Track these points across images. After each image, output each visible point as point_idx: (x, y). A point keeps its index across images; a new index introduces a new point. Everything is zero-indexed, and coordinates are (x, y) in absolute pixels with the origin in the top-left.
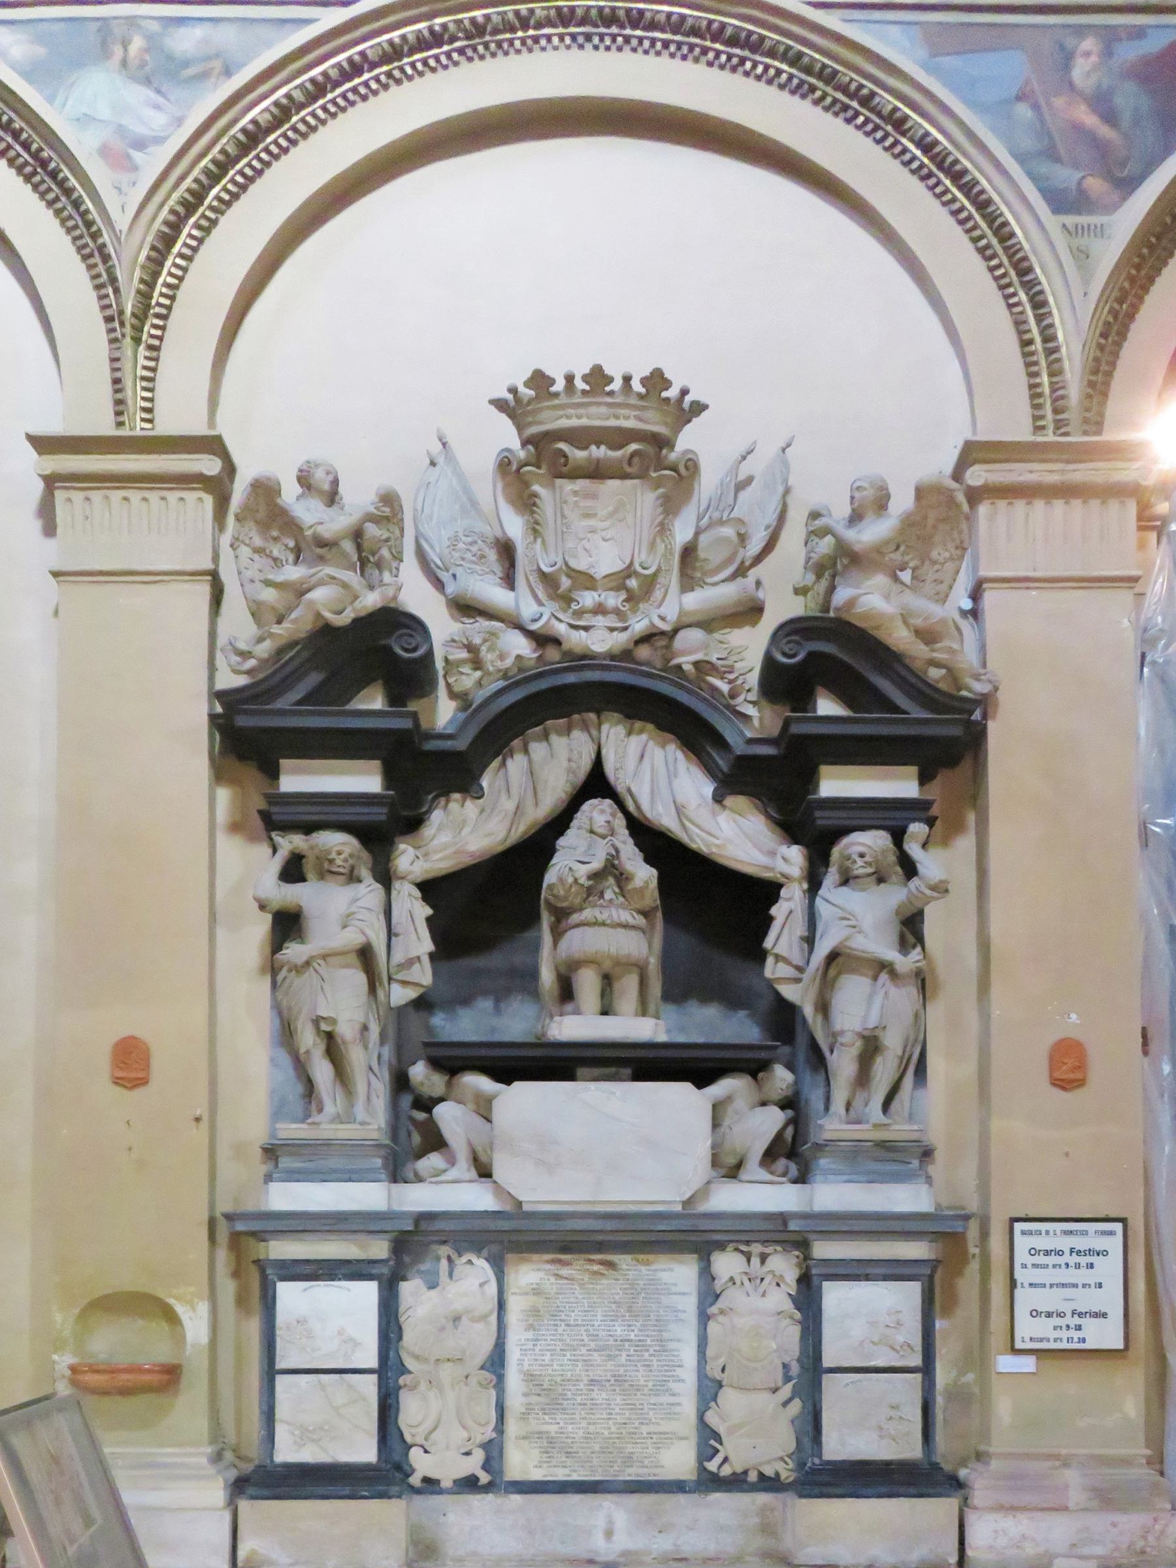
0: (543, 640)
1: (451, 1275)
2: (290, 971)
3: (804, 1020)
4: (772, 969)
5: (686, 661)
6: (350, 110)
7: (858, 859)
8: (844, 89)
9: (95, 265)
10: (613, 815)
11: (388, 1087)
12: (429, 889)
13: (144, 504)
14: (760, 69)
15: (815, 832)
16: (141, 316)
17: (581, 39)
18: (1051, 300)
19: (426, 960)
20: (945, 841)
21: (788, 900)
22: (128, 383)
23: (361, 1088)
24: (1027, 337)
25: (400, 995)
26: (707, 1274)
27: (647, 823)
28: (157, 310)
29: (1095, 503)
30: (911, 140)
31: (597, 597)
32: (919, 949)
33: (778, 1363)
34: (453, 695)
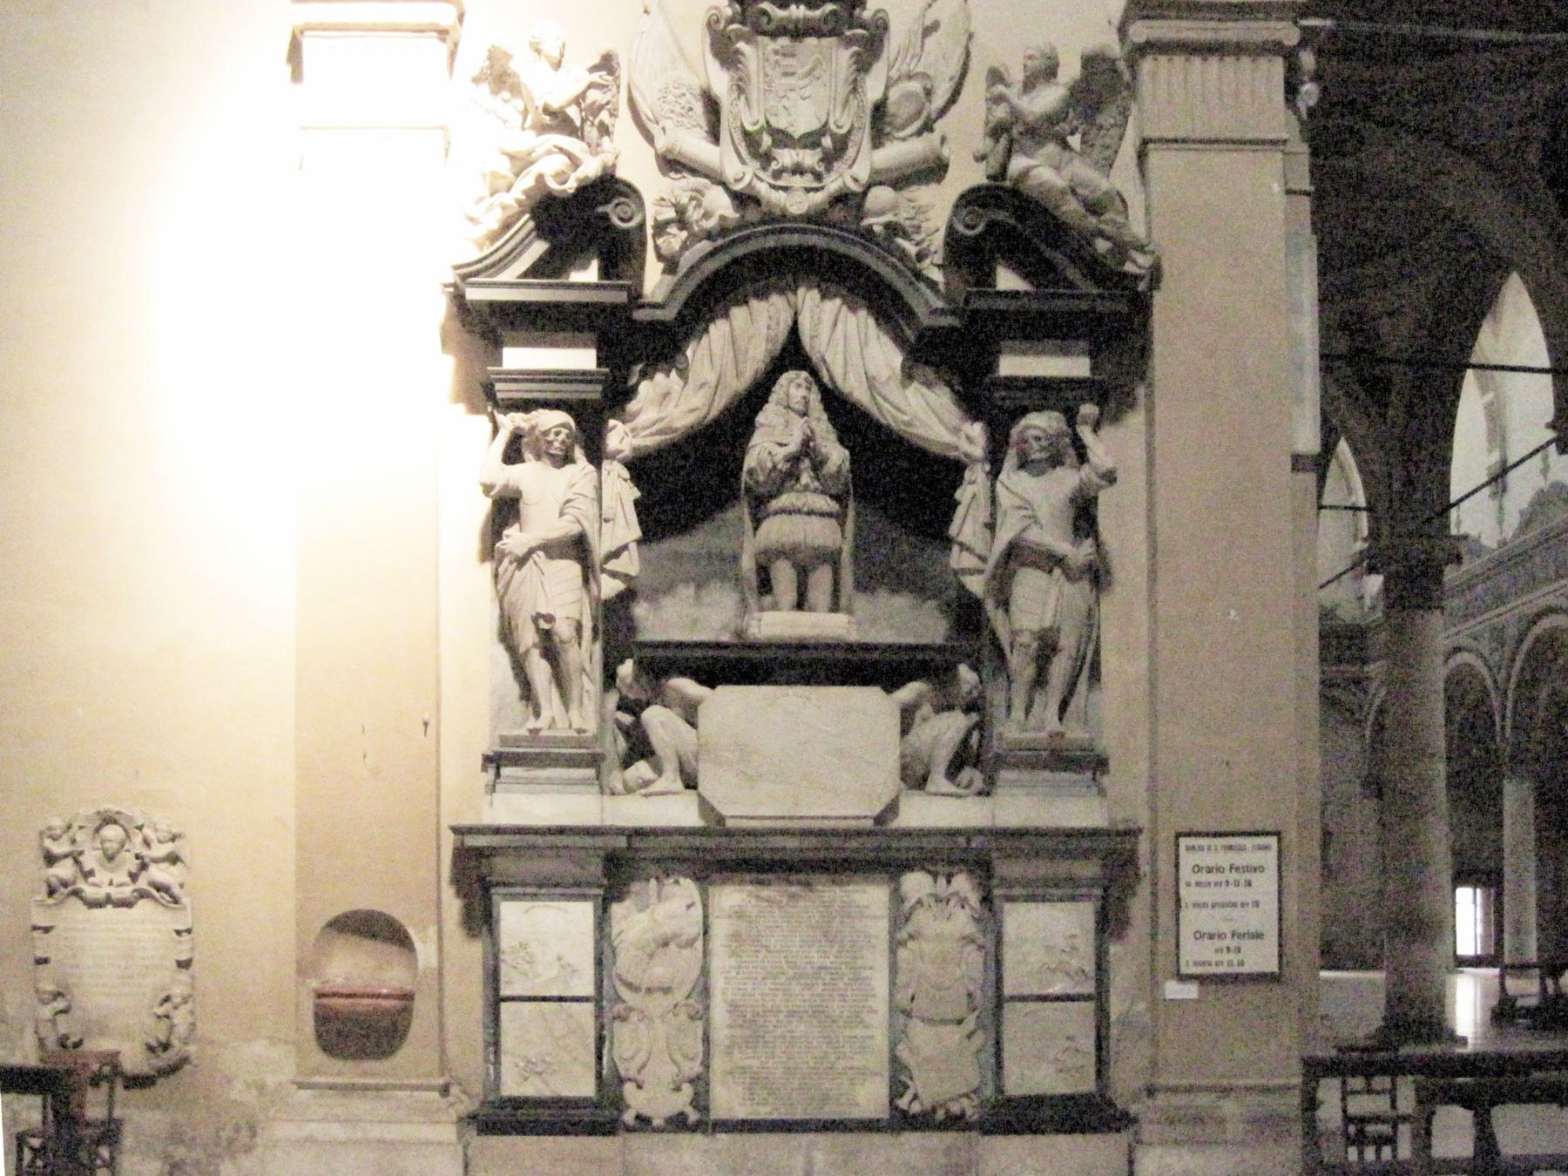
0: (743, 199)
1: (659, 895)
4: (958, 559)
5: (876, 223)
12: (640, 468)
19: (633, 546)
20: (1115, 419)
21: (973, 482)
25: (610, 587)
26: (897, 897)
32: (1090, 541)
33: (963, 992)
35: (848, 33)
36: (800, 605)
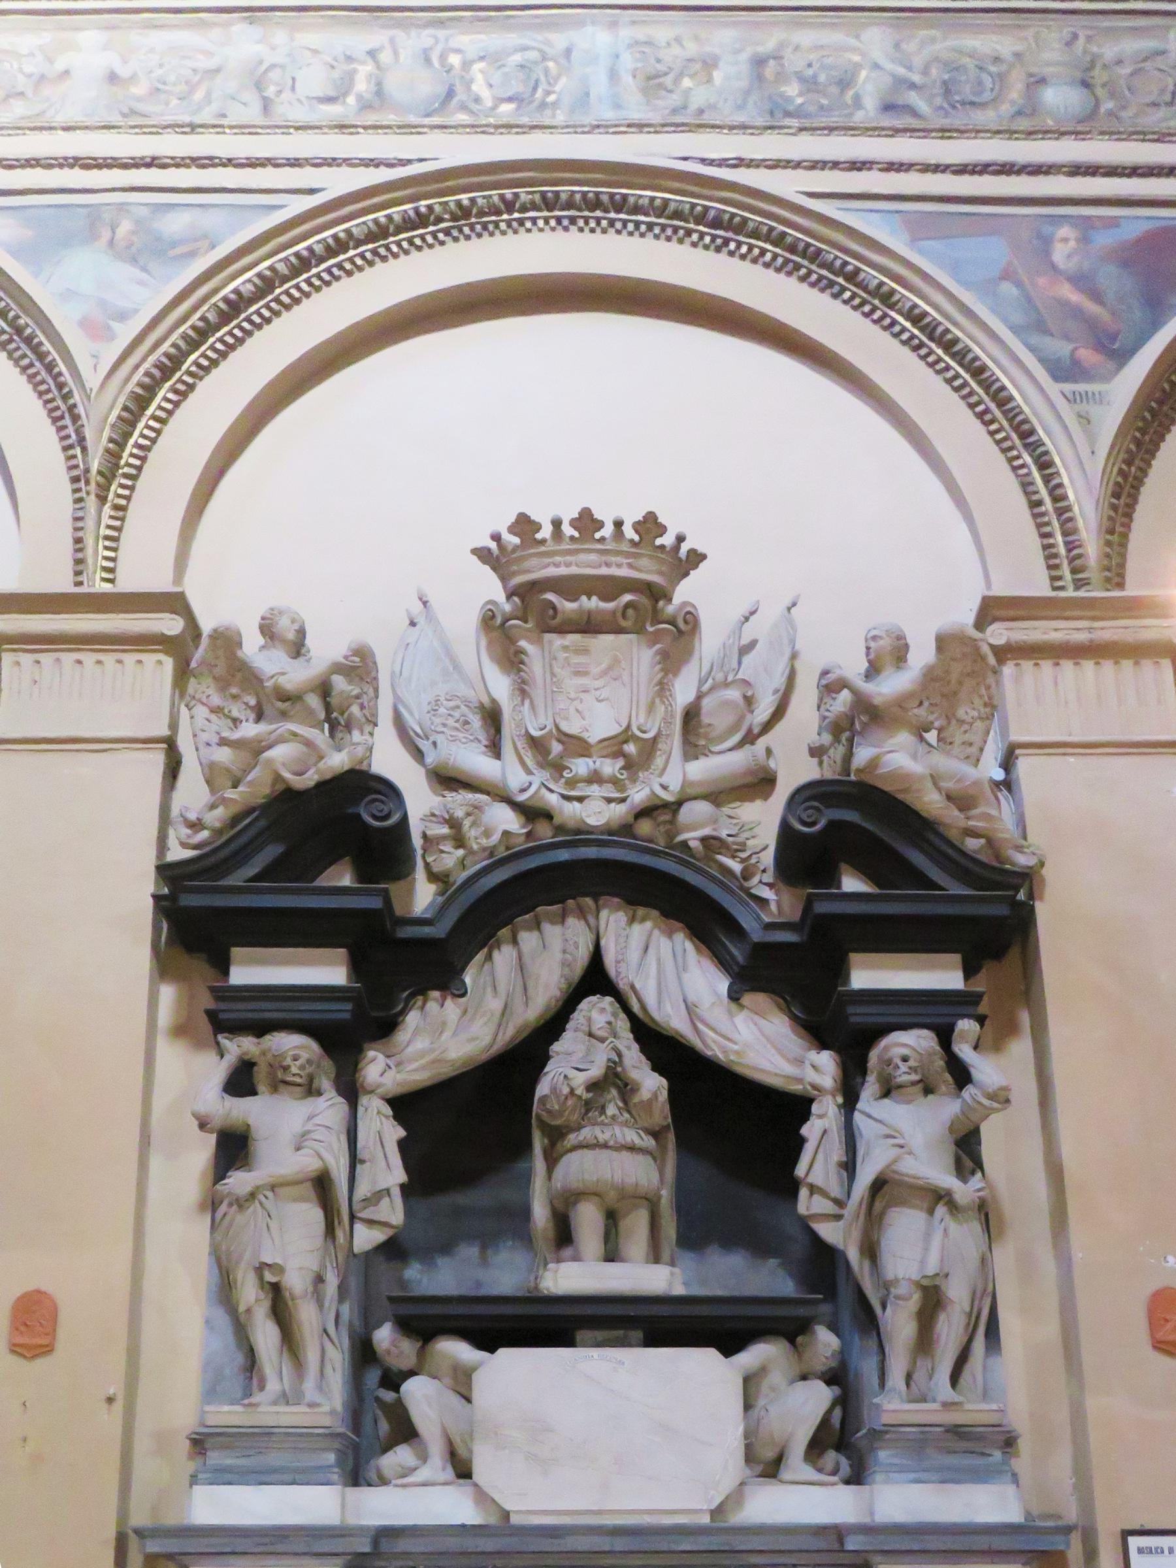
0: (532, 813)
2: (230, 1205)
3: (847, 1262)
4: (806, 1204)
5: (692, 837)
6: (335, 284)
7: (900, 1064)
8: (829, 266)
9: (66, 427)
10: (614, 1015)
11: (347, 1356)
12: (403, 1106)
13: (98, 668)
14: (744, 249)
15: (846, 1030)
16: (108, 475)
17: (566, 222)
18: (1057, 460)
19: (396, 1192)
21: (820, 1117)
22: (89, 541)
23: (312, 1356)
24: (1035, 497)
25: (366, 1238)
27: (651, 1024)
28: (126, 470)
29: (1127, 664)
30: (900, 312)
31: (591, 763)
34: (433, 877)
35: (651, 629)
36: (611, 1255)
